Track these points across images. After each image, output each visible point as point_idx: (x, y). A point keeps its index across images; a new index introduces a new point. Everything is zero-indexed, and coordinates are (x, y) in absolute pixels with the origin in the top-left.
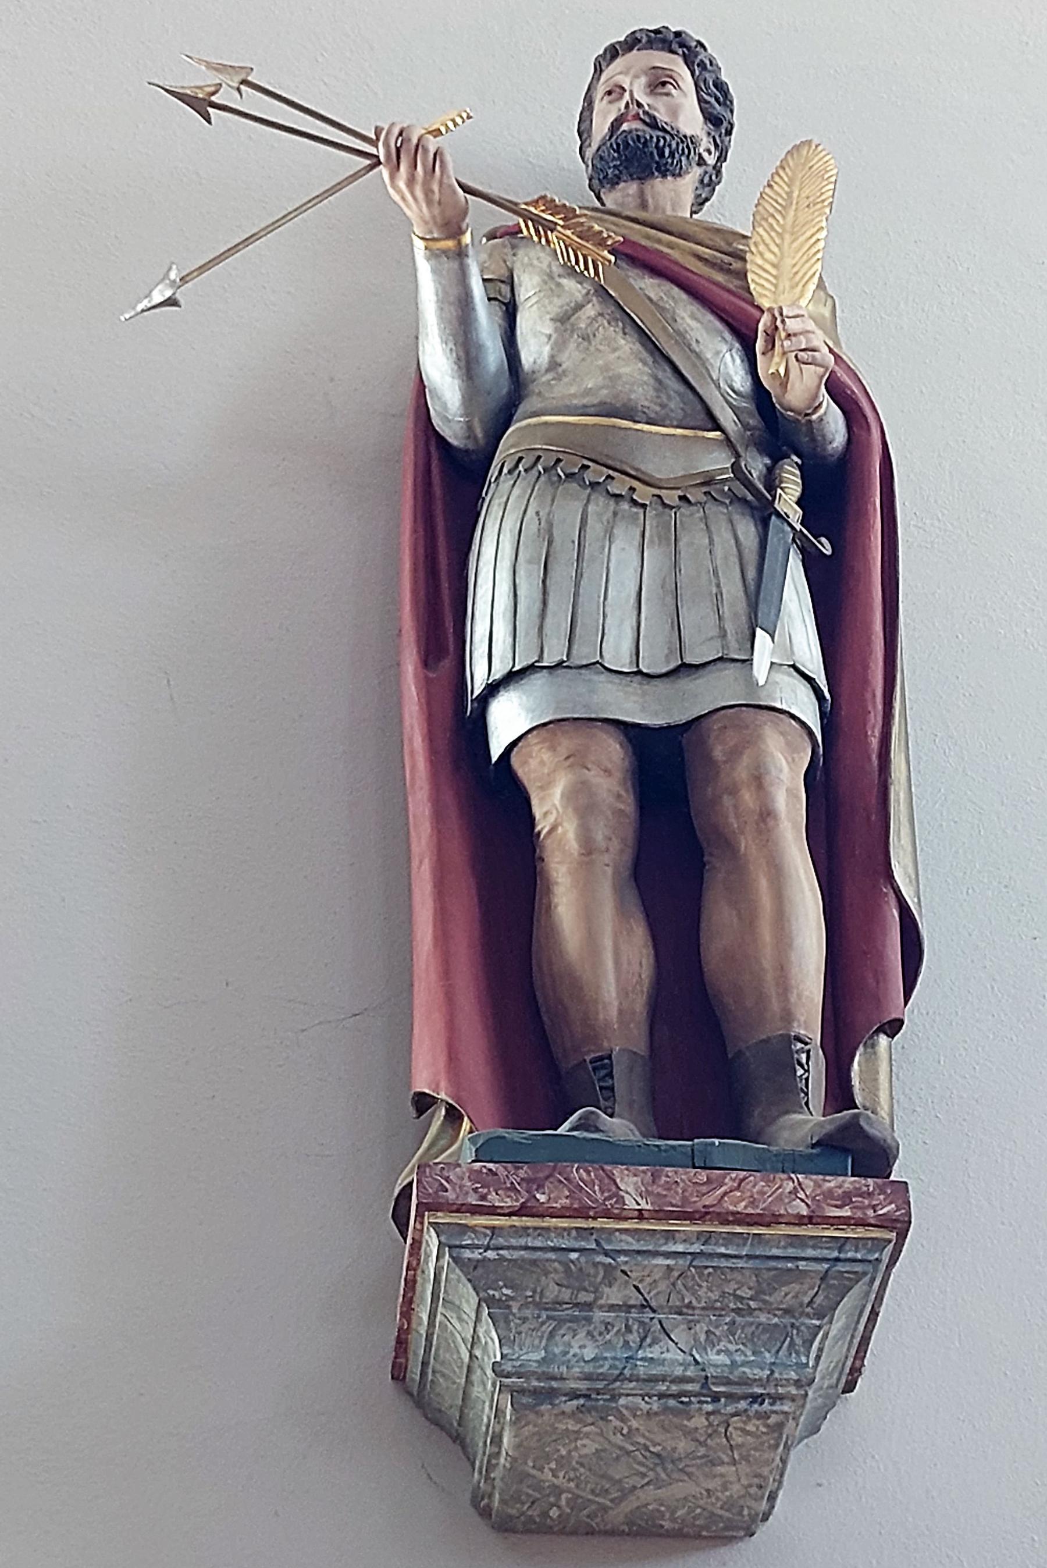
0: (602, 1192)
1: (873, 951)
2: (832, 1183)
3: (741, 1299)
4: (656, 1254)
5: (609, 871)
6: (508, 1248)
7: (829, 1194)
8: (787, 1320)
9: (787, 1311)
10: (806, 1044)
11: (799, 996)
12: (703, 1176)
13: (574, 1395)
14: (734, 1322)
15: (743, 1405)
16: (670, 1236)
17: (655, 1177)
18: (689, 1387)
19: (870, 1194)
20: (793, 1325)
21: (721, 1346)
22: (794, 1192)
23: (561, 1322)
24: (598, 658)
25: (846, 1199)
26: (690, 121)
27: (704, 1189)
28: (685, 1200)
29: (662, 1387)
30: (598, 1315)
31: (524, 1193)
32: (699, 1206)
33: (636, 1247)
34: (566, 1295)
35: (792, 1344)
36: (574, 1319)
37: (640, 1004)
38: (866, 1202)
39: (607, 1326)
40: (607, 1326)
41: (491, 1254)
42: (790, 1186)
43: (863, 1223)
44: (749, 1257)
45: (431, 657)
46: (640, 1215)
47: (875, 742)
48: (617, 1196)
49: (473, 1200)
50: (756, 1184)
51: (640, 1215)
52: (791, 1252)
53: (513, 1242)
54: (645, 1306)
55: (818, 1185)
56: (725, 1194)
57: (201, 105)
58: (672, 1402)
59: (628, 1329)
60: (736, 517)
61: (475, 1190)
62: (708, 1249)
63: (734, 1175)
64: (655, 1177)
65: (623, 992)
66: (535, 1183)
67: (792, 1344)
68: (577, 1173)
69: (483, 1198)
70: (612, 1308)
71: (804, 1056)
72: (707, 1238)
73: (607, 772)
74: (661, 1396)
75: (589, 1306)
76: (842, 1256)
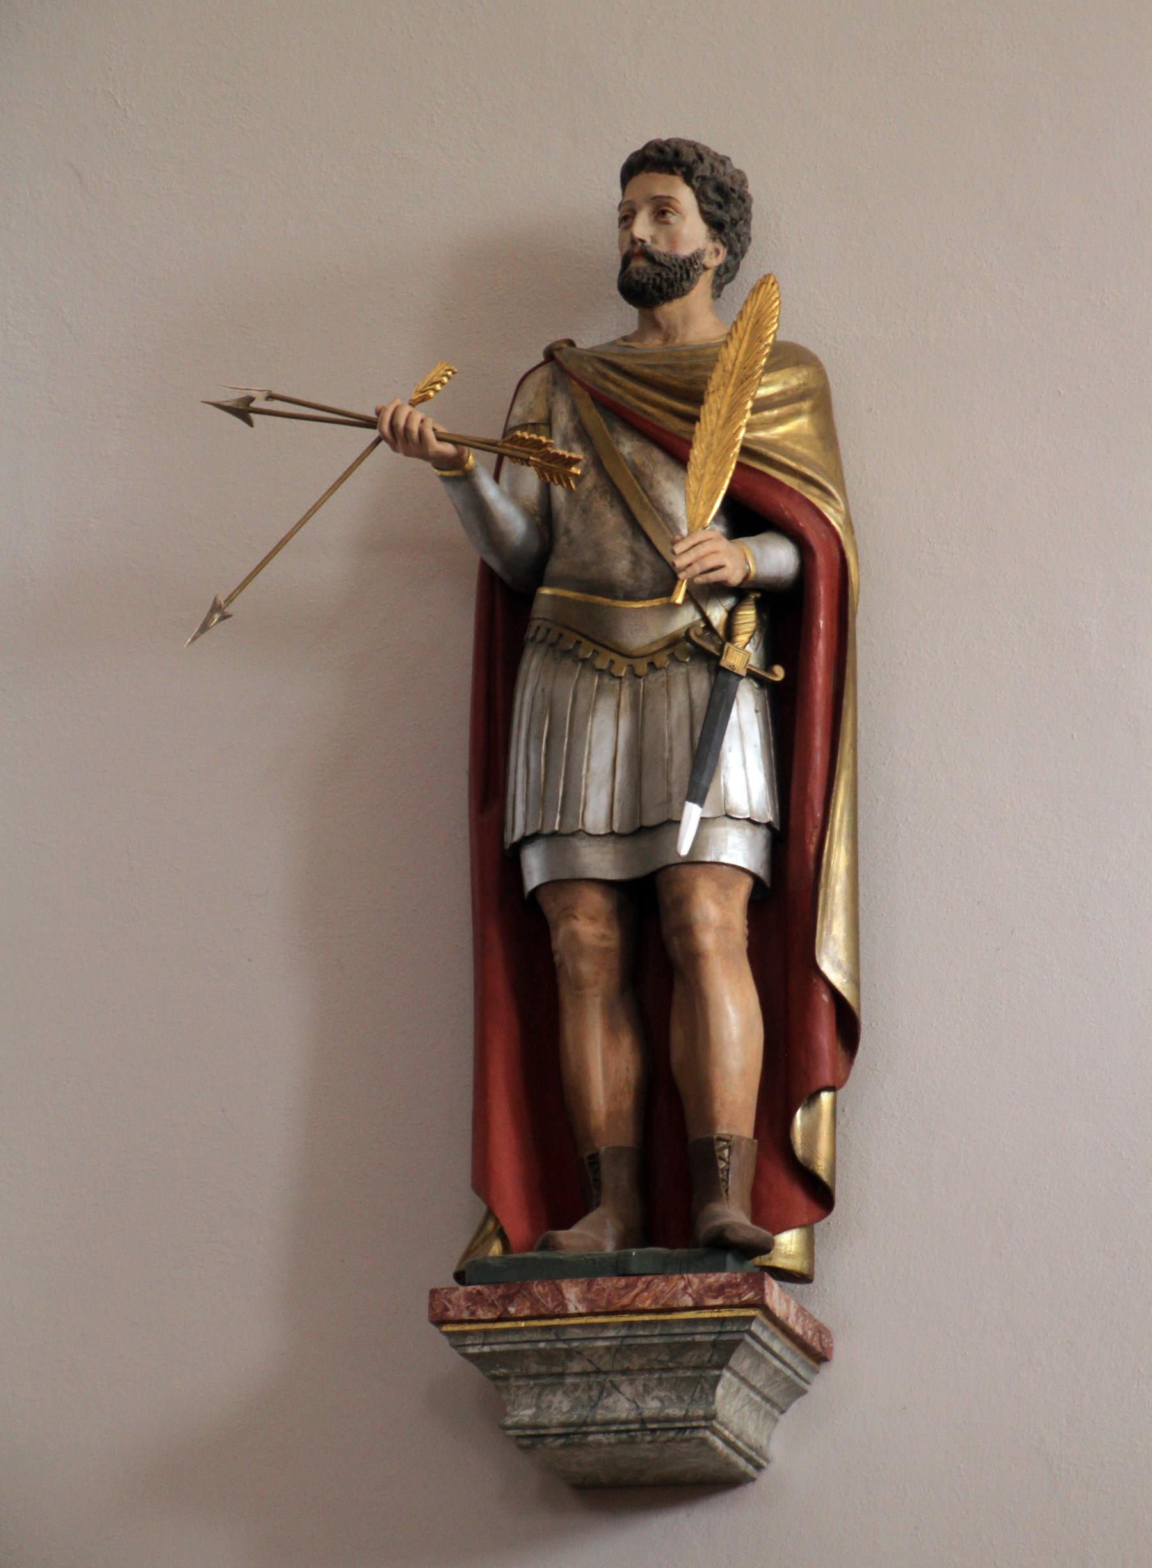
0: (553, 1301)
1: (809, 1031)
2: (712, 1279)
3: (661, 1362)
4: (597, 1339)
5: (598, 1000)
6: (498, 1344)
7: (709, 1288)
8: (696, 1374)
9: (695, 1368)
10: (728, 1141)
11: (722, 1105)
12: (623, 1282)
13: (558, 1436)
14: (660, 1378)
15: (672, 1434)
16: (604, 1326)
17: (590, 1285)
18: (632, 1427)
19: (737, 1285)
20: (701, 1376)
21: (655, 1393)
22: (685, 1288)
23: (544, 1386)
24: (580, 827)
25: (720, 1290)
26: (691, 233)
27: (622, 1292)
28: (609, 1302)
29: (614, 1428)
30: (569, 1380)
31: (500, 1307)
32: (618, 1305)
33: (582, 1336)
34: (543, 1369)
35: (702, 1389)
36: (551, 1385)
37: (627, 1103)
38: (734, 1292)
39: (576, 1387)
40: (576, 1387)
41: (486, 1349)
42: (682, 1284)
43: (732, 1307)
44: (660, 1335)
45: (711, 457)
46: (580, 1315)
47: (812, 849)
48: (562, 1303)
49: (466, 1315)
50: (660, 1284)
51: (580, 1315)
52: (688, 1329)
53: (500, 1339)
54: (598, 1372)
55: (702, 1282)
56: (637, 1295)
57: (243, 411)
58: (624, 1436)
59: (590, 1388)
60: (693, 674)
61: (468, 1308)
62: (633, 1332)
63: (644, 1279)
64: (590, 1285)
65: (613, 1097)
66: (508, 1299)
67: (702, 1389)
68: (537, 1289)
69: (473, 1313)
70: (577, 1374)
71: (726, 1152)
72: (630, 1325)
73: (593, 919)
74: (618, 1432)
75: (562, 1375)
76: (724, 1329)
